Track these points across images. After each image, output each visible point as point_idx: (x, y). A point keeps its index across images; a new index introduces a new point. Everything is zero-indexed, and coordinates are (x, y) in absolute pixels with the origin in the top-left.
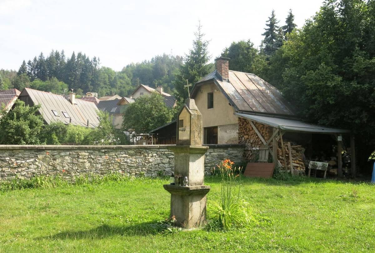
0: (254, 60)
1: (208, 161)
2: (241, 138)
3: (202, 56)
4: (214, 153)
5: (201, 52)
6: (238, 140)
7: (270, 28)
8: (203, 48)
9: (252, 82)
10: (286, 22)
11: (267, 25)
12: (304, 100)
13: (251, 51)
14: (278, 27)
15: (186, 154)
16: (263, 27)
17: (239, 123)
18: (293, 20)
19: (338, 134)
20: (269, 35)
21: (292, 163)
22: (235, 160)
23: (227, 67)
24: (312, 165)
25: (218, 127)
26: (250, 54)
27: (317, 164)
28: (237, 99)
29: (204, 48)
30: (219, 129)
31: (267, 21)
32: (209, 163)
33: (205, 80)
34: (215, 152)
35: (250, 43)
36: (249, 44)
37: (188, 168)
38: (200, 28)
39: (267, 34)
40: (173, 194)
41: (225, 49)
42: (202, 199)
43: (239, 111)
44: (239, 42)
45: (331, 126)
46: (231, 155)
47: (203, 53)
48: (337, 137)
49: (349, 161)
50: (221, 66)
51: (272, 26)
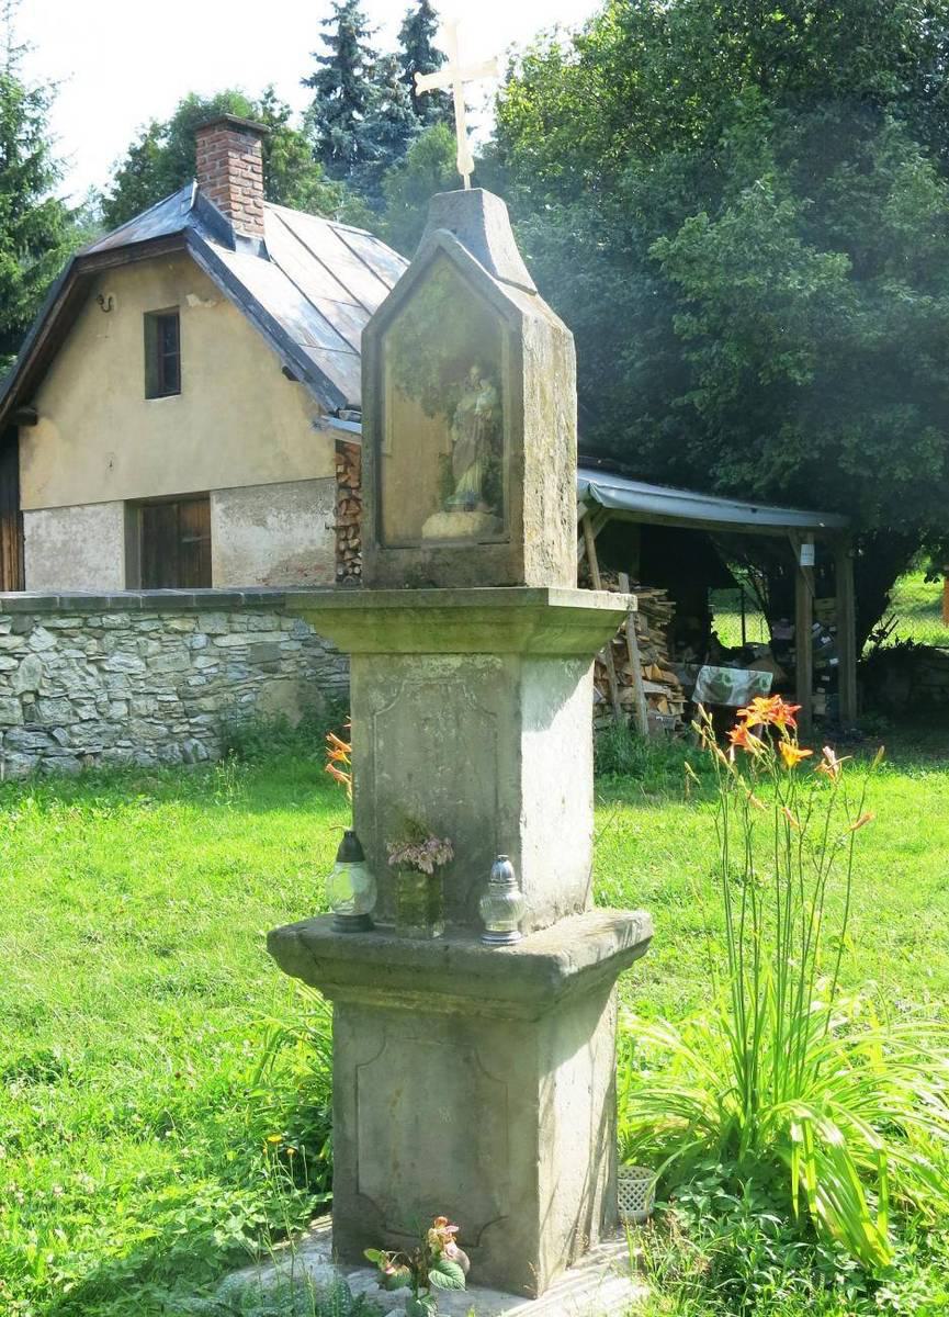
0: (298, 184)
1: (202, 680)
2: (348, 555)
3: (25, 153)
4: (230, 636)
5: (22, 136)
6: (332, 566)
7: (335, 54)
8: (27, 113)
9: (369, 267)
10: (403, 37)
11: (328, 40)
12: (638, 365)
13: (280, 140)
14: (373, 55)
15: (479, 662)
16: (307, 52)
17: (339, 475)
18: (433, 32)
19: (801, 533)
20: (331, 89)
21: (638, 680)
22: (333, 670)
23: (254, 176)
24: (710, 687)
25: (214, 498)
26: (277, 158)
27: (728, 680)
28: (322, 345)
29: (34, 115)
30: (217, 508)
31: (324, 22)
32: (205, 694)
33: (136, 238)
34: (234, 632)
35: (276, 106)
36: (272, 110)
37: (506, 786)
38: (12, 10)
39: (324, 83)
40: (355, 1006)
41: (149, 125)
42: (597, 1020)
43: (348, 408)
44: (219, 97)
45: (776, 496)
46: (316, 645)
47: (32, 141)
48: (800, 550)
49: (834, 661)
50: (226, 163)
51: (350, 45)
